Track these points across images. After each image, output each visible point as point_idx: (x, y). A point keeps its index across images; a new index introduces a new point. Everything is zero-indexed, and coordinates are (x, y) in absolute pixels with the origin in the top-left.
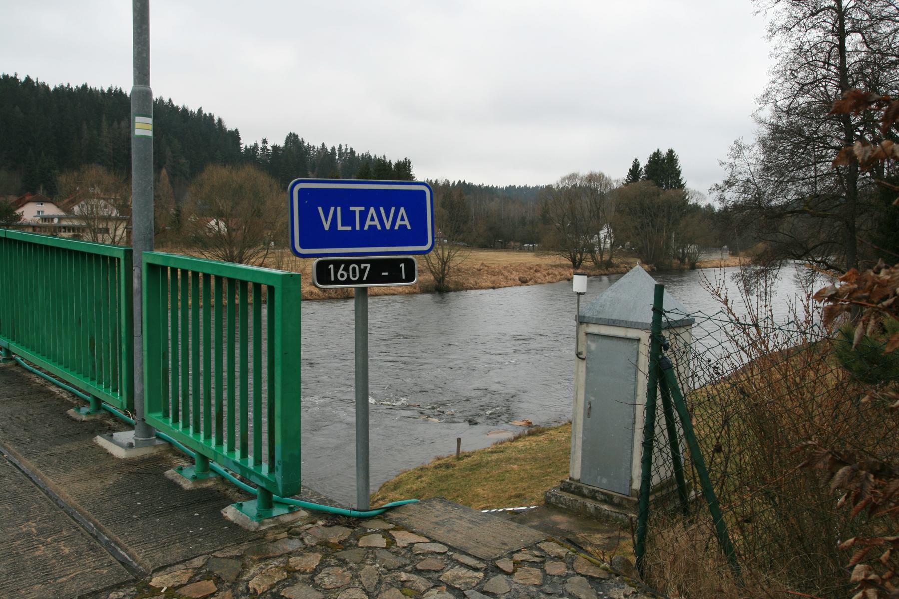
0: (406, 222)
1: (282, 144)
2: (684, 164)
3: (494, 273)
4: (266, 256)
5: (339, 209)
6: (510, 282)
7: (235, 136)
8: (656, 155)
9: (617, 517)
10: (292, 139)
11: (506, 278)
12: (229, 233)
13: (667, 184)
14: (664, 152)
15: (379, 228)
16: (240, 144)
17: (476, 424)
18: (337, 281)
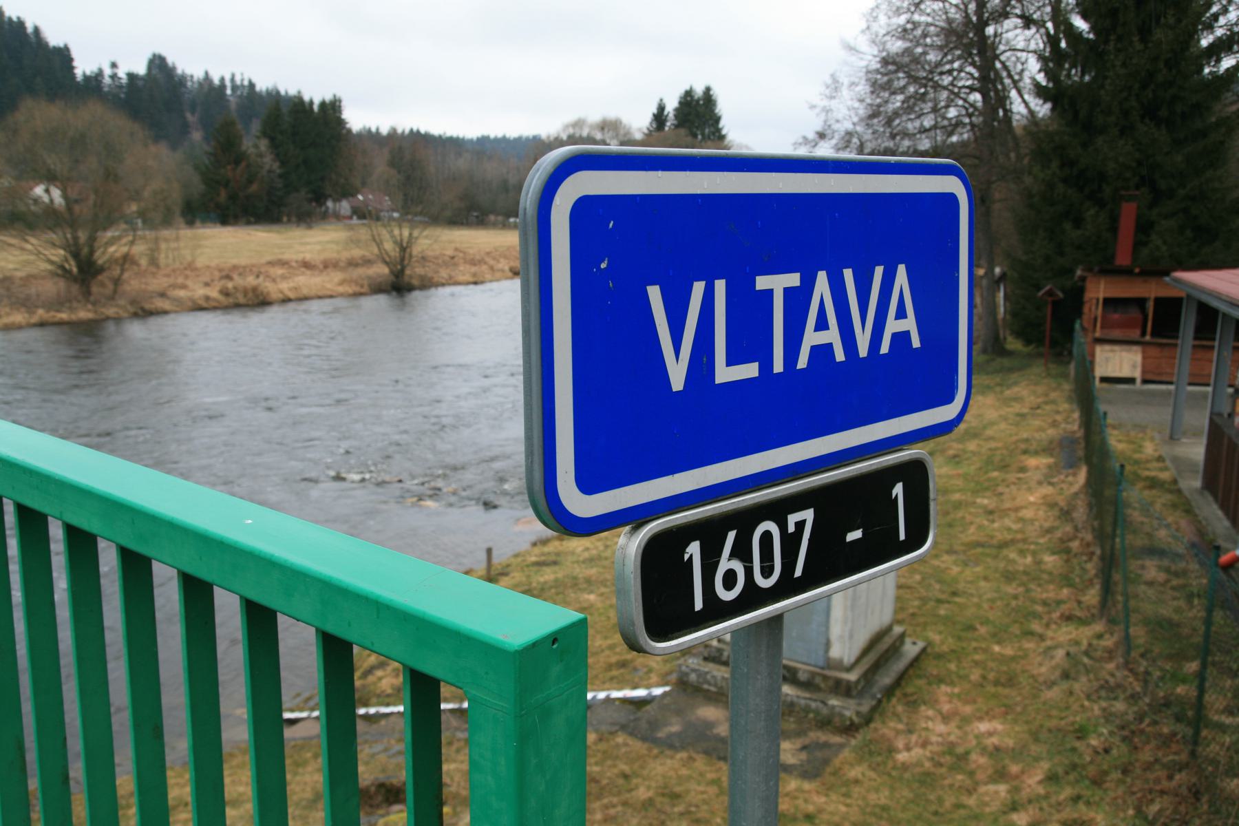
0: (909, 324)
1: (141, 69)
2: (725, 108)
3: (473, 262)
4: (132, 243)
5: (720, 286)
6: (498, 275)
7: (63, 56)
8: (689, 93)
9: (808, 706)
10: (158, 63)
11: (492, 268)
12: (69, 207)
13: (703, 135)
14: (699, 91)
15: (840, 356)
16: (73, 68)
17: (495, 507)
18: (717, 611)
